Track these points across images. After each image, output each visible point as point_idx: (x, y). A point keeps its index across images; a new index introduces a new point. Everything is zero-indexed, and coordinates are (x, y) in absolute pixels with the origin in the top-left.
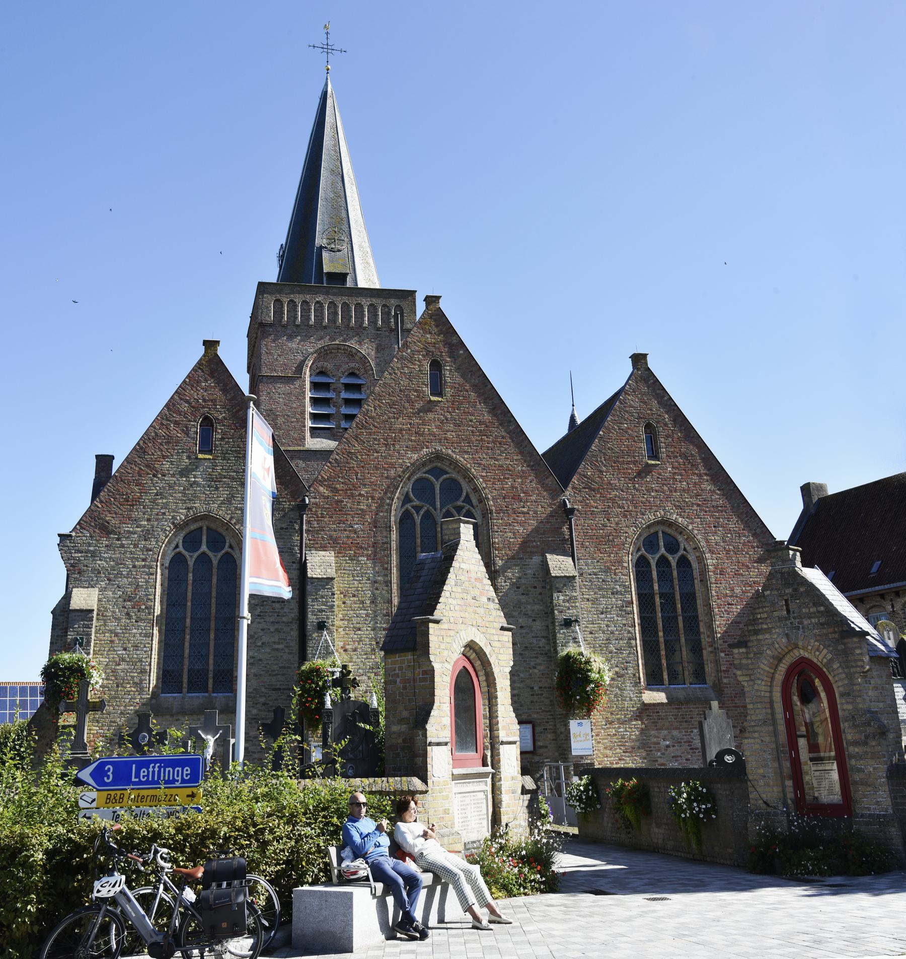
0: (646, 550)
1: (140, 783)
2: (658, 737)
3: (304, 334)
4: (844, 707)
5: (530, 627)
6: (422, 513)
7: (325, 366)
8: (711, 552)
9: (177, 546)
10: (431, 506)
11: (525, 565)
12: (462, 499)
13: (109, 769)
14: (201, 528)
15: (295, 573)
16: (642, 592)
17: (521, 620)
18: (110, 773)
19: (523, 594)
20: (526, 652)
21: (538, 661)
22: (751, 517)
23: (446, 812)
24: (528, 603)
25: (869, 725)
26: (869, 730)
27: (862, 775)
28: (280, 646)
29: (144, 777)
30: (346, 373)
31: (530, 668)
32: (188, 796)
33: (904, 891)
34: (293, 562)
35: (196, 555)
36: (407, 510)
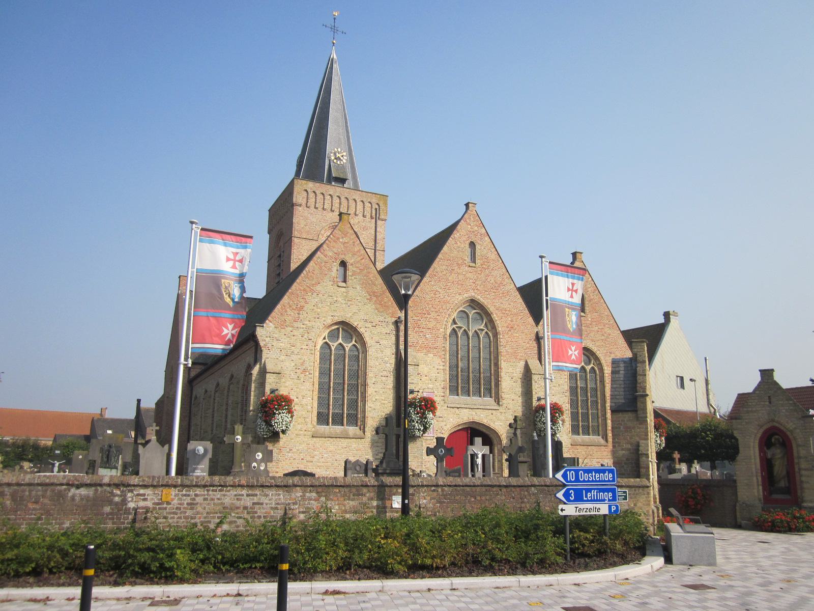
1: (588, 501)
9: (324, 338)
13: (572, 493)
15: (259, 352)
16: (321, 411)
18: (572, 495)
19: (514, 382)
29: (589, 497)
32: (564, 510)
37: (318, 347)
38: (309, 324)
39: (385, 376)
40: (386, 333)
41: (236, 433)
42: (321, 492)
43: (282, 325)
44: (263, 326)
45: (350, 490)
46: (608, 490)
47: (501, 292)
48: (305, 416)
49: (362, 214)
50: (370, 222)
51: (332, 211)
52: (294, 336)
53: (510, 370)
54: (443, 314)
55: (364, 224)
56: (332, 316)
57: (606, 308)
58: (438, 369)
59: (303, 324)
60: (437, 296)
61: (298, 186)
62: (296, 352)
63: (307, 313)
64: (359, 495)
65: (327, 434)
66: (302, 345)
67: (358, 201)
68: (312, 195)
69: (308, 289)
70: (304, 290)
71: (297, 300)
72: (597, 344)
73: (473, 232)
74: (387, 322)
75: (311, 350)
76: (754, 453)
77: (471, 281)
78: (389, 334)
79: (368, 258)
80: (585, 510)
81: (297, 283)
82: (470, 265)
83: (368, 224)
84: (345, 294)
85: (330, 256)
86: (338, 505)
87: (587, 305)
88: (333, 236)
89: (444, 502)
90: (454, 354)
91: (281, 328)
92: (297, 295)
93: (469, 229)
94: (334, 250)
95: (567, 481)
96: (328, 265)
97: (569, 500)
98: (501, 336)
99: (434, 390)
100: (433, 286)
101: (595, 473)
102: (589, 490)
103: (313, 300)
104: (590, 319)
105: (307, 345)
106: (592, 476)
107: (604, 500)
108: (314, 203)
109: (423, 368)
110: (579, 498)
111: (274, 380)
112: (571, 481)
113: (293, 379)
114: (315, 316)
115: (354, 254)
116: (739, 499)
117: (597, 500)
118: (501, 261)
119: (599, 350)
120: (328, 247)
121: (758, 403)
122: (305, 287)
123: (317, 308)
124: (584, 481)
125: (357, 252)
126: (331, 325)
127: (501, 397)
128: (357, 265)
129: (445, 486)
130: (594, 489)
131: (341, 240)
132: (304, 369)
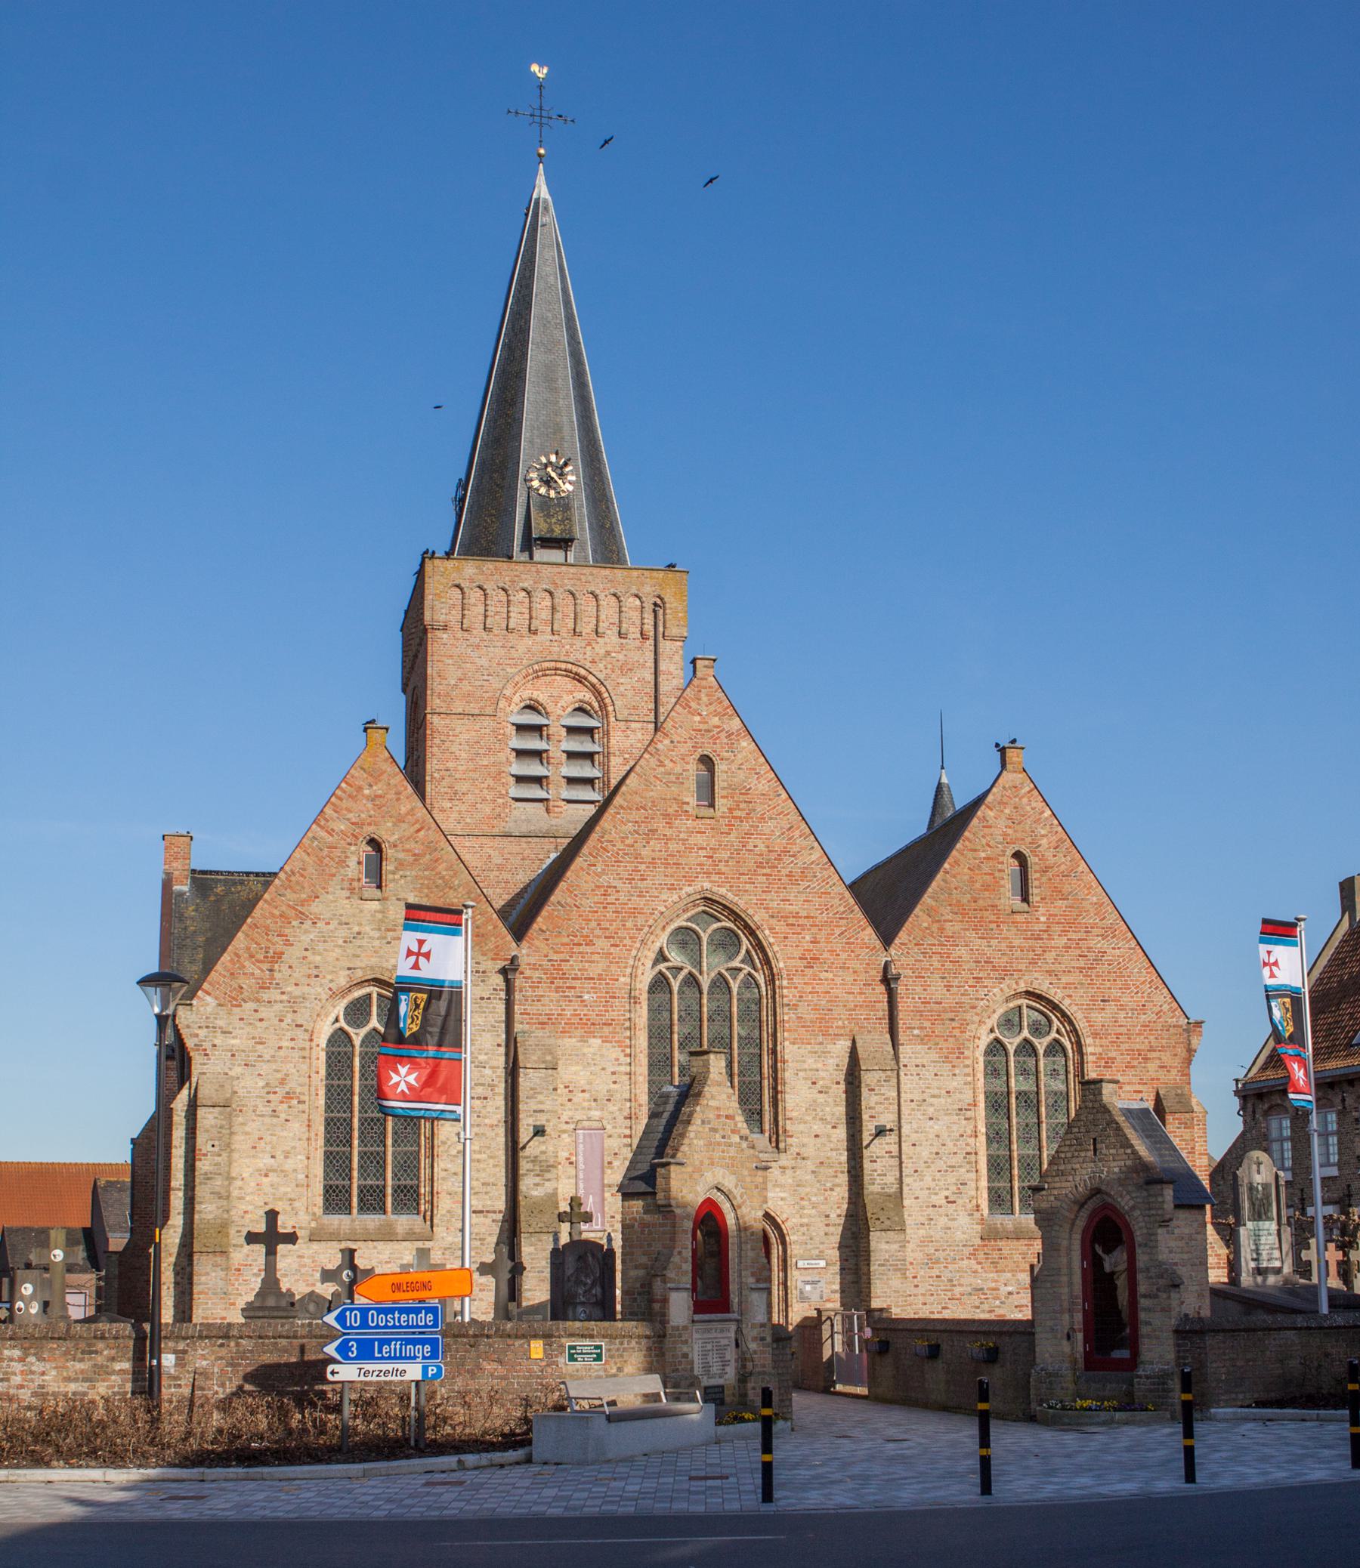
0: (348, 1023)
1: (383, 1358)
2: (996, 1281)
3: (501, 644)
4: (1142, 1259)
5: (829, 1136)
6: (681, 977)
7: (534, 696)
8: (1095, 1035)
9: (337, 1020)
10: (695, 967)
11: (824, 1052)
12: (740, 957)
14: (369, 996)
17: (815, 1127)
18: (354, 1349)
19: (821, 1092)
20: (822, 1169)
21: (837, 1181)
22: (1156, 988)
23: (685, 1356)
24: (827, 1103)
25: (1162, 1277)
26: (1162, 1282)
27: (1149, 1328)
28: (484, 1156)
30: (570, 709)
31: (826, 1190)
33: (3, 1160)
34: (499, 1045)
35: (363, 1031)
36: (660, 973)
37: (323, 1041)
38: (297, 992)
39: (479, 1098)
40: (482, 999)
41: (52, 1245)
42: (29, 1349)
43: (233, 1000)
44: (191, 1005)
45: (77, 1344)
46: (423, 1342)
47: (784, 872)
48: (293, 1196)
49: (615, 629)
50: (639, 648)
51: (532, 632)
52: (261, 1020)
53: (810, 1062)
54: (627, 942)
55: (621, 657)
56: (349, 969)
57: (1094, 884)
58: (614, 1073)
59: (283, 993)
60: (611, 899)
61: (437, 578)
62: (267, 1057)
63: (290, 967)
64: (91, 1352)
65: (345, 1234)
66: (281, 1039)
67: (601, 597)
68: (475, 596)
69: (291, 913)
70: (281, 916)
71: (268, 940)
72: (1064, 979)
73: (708, 731)
74: (484, 972)
75: (303, 1049)
76: (1070, 1263)
77: (702, 853)
78: (489, 998)
79: (434, 825)
80: (376, 1373)
81: (266, 901)
82: (700, 815)
83: (635, 656)
84: (379, 916)
85: (342, 831)
86: (55, 1368)
87: (1036, 883)
88: (347, 783)
89: (240, 1365)
90: (659, 1034)
91: (232, 1006)
92: (267, 928)
93: (696, 726)
94: (350, 816)
95: (344, 1326)
96: (337, 853)
97: (347, 1358)
98: (785, 983)
99: (605, 1122)
100: (599, 875)
101: (400, 1313)
102: (388, 1342)
103: (304, 936)
104: (1043, 919)
105: (292, 1039)
106: (394, 1319)
107: (415, 1357)
108: (481, 618)
109: (570, 1072)
110: (366, 1352)
111: (213, 1122)
112: (351, 1327)
113: (263, 1116)
114: (310, 972)
115: (400, 820)
116: (1038, 1361)
117: (401, 1358)
118: (784, 795)
119: (1070, 996)
120: (336, 812)
121: (1076, 1154)
122: (284, 908)
123: (314, 953)
124: (377, 1326)
125: (408, 814)
126: (350, 989)
127: (785, 1131)
128: (408, 847)
129: (241, 1338)
130: (397, 1340)
131: (367, 792)
132: (288, 1093)
